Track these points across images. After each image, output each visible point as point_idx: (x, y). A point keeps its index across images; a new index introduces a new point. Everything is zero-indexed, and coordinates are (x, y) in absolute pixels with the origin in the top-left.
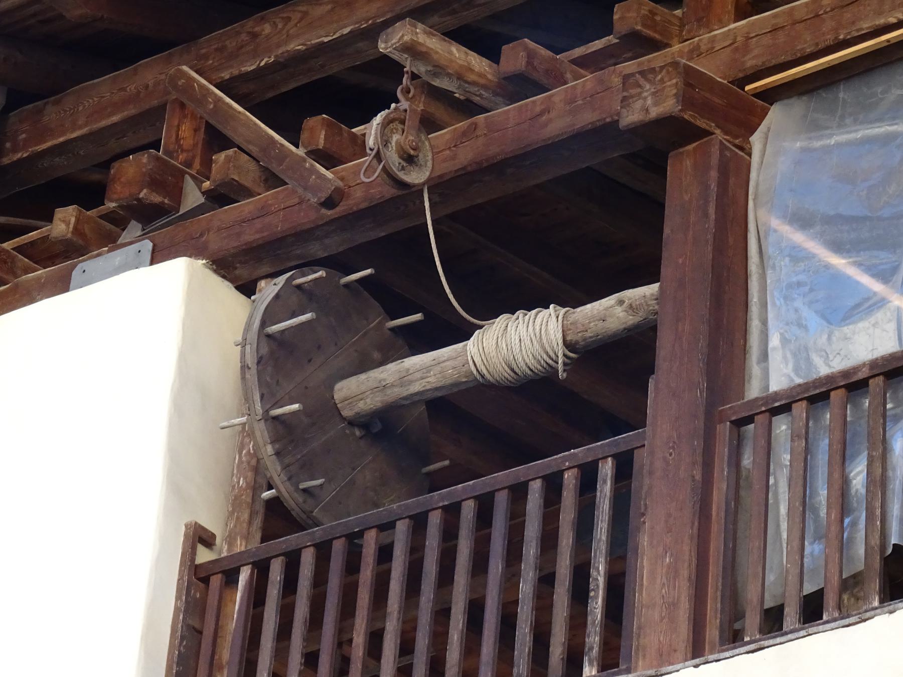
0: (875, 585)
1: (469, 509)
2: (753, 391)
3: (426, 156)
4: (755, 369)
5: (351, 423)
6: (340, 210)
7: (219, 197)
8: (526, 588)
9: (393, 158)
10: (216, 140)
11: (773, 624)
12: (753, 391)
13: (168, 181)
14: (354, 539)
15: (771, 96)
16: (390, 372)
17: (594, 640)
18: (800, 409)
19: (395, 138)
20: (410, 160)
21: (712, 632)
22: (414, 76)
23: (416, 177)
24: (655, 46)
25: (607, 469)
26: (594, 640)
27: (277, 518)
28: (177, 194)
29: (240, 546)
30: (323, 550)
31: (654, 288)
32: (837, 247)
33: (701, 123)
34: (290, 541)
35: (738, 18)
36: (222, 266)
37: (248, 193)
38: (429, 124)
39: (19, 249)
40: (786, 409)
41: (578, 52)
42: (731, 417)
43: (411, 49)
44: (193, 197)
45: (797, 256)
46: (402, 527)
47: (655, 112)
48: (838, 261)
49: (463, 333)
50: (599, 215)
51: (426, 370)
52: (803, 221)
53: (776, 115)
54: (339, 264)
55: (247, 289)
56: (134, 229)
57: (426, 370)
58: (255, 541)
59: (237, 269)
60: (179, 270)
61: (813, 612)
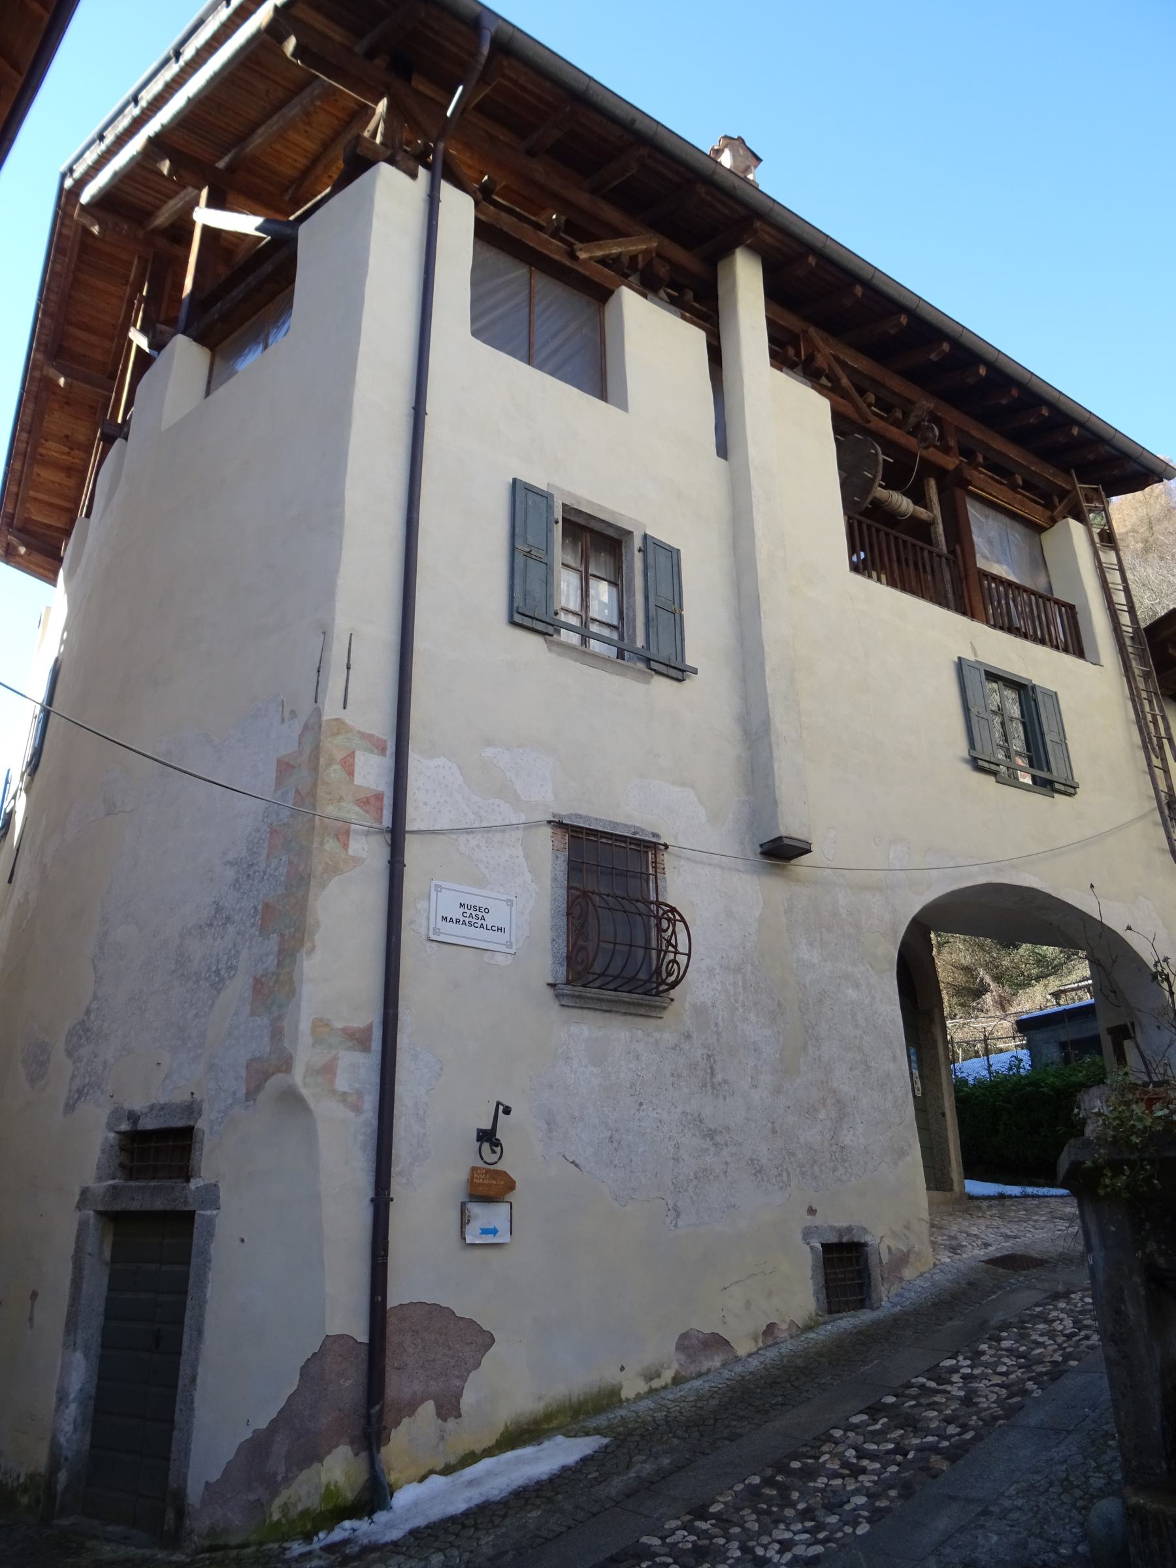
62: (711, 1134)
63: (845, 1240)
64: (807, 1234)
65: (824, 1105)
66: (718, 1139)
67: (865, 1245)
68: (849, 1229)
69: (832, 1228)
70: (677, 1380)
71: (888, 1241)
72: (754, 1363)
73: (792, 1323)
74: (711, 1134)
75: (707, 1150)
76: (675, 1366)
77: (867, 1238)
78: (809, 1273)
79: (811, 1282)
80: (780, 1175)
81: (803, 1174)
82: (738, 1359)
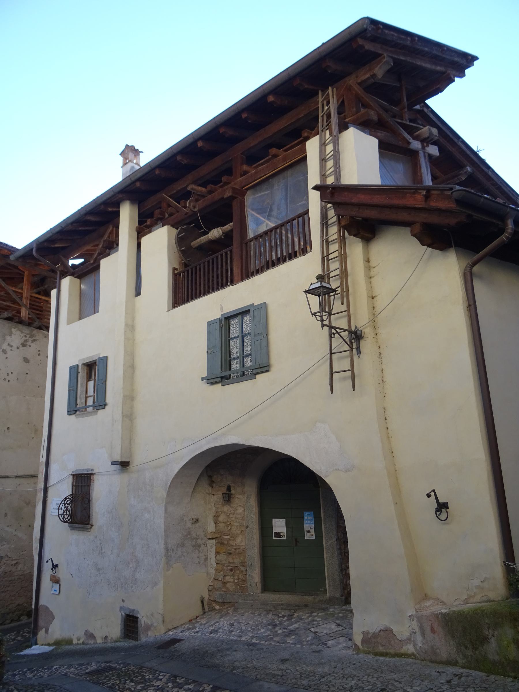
0: (265, 267)
1: (211, 261)
2: (248, 238)
3: (197, 206)
4: (248, 235)
5: (195, 248)
6: (188, 215)
7: (171, 215)
8: (219, 272)
9: (191, 207)
10: (169, 206)
11: (252, 275)
12: (248, 238)
13: (162, 214)
14: (196, 267)
15: (247, 189)
16: (198, 240)
17: (229, 279)
18: (254, 240)
19: (192, 204)
20: (194, 207)
21: (244, 276)
22: (194, 193)
23: (196, 210)
24: (229, 183)
25: (229, 252)
26: (229, 279)
27: (186, 265)
28: (164, 215)
29: (181, 270)
30: (192, 269)
31: (232, 223)
32: (258, 214)
33: (236, 196)
34: (187, 268)
35: (241, 177)
36: (173, 226)
37: (174, 214)
38: (197, 200)
39: (144, 226)
40: (252, 241)
41: (219, 185)
42: (245, 243)
43: (192, 189)
44: (167, 216)
45: (252, 215)
46: (202, 265)
47: (229, 195)
48: (258, 216)
49: (208, 233)
50: (226, 211)
51: (203, 239)
52: (253, 210)
53: (249, 192)
54: (190, 223)
55: (177, 229)
56: (159, 222)
57: (203, 239)
58: (184, 268)
59: (174, 225)
60: (166, 227)
61: (125, 332)
62: (99, 570)
63: (131, 614)
64: (121, 608)
65: (132, 562)
66: (101, 572)
67: (137, 618)
68: (133, 610)
69: (128, 609)
70: (83, 643)
71: (145, 619)
72: (101, 645)
73: (112, 638)
74: (99, 570)
75: (97, 575)
76: (83, 639)
77: (138, 616)
78: (119, 622)
79: (120, 626)
80: (115, 586)
81: (122, 587)
82: (97, 643)
